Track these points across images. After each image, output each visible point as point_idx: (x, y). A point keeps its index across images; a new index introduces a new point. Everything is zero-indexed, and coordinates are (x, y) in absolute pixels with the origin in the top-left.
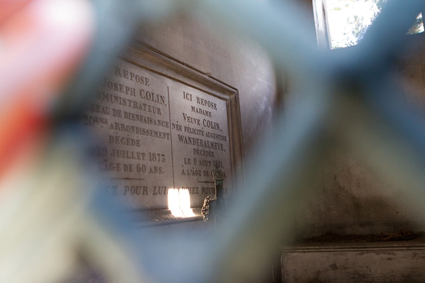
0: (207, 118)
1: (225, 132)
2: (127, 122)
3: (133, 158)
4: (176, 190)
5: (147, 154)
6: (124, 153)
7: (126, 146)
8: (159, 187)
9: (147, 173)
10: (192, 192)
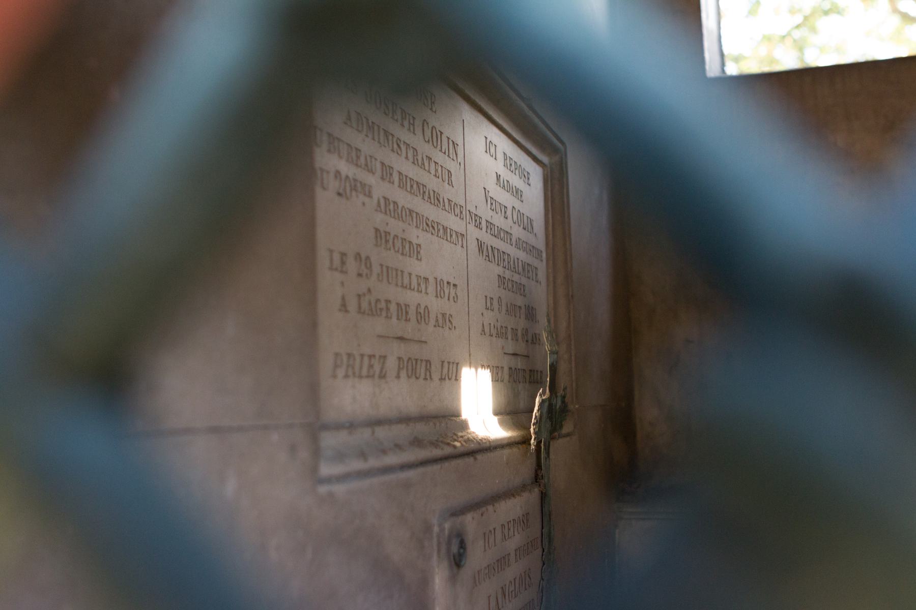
0: (517, 204)
1: (540, 242)
2: (404, 199)
3: (410, 288)
4: (473, 370)
5: (431, 280)
6: (397, 275)
7: (401, 257)
8: (449, 363)
9: (431, 328)
10: (496, 380)
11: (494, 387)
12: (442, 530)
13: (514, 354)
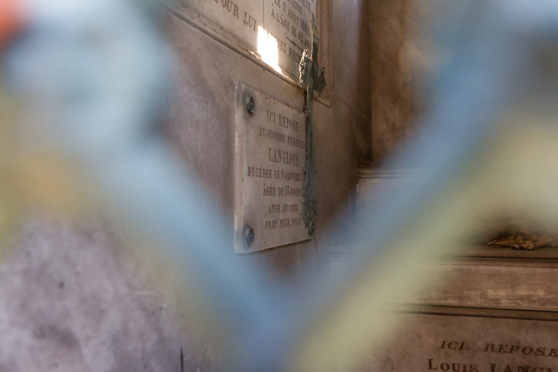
11: (280, 54)
12: (240, 88)
13: (293, 42)
